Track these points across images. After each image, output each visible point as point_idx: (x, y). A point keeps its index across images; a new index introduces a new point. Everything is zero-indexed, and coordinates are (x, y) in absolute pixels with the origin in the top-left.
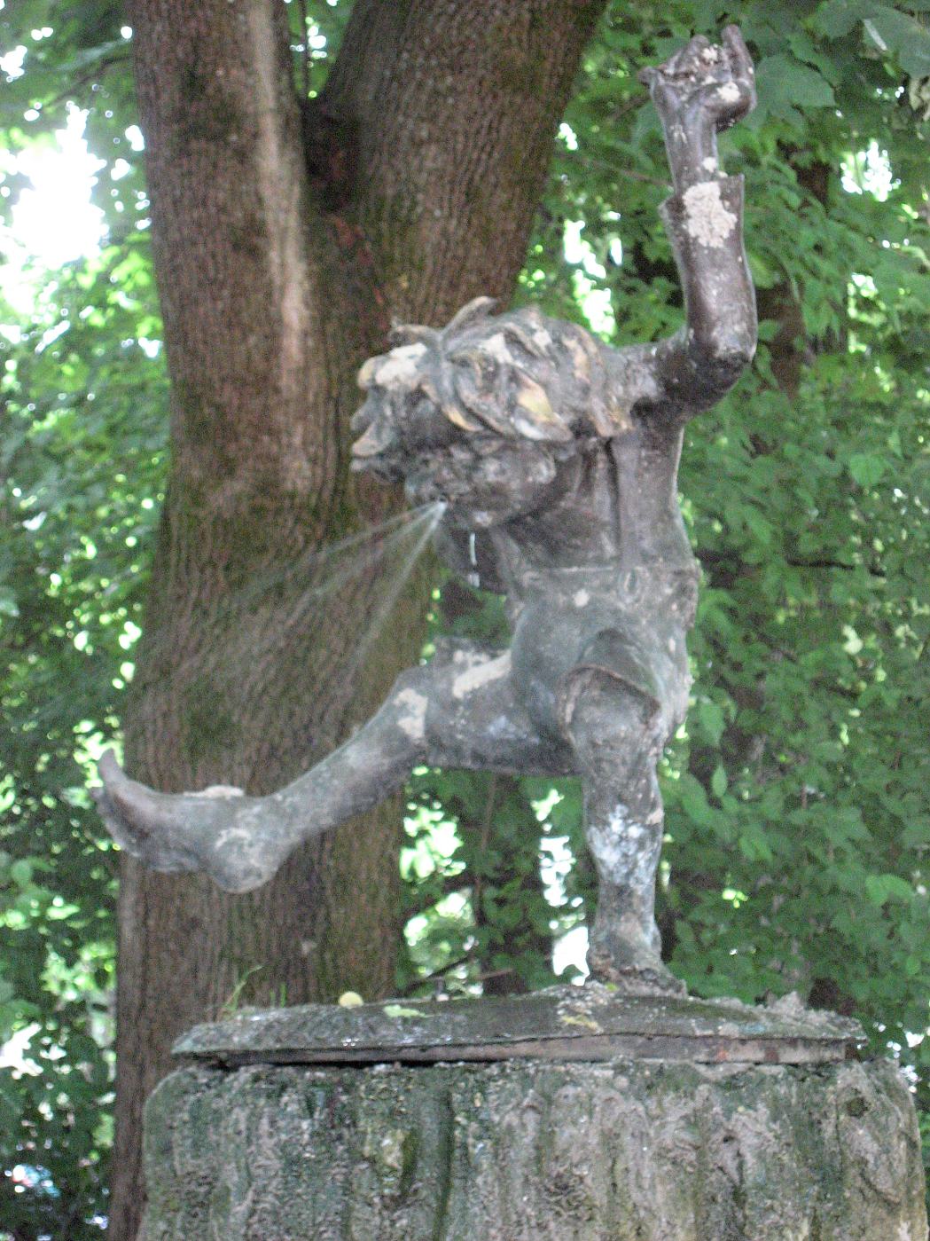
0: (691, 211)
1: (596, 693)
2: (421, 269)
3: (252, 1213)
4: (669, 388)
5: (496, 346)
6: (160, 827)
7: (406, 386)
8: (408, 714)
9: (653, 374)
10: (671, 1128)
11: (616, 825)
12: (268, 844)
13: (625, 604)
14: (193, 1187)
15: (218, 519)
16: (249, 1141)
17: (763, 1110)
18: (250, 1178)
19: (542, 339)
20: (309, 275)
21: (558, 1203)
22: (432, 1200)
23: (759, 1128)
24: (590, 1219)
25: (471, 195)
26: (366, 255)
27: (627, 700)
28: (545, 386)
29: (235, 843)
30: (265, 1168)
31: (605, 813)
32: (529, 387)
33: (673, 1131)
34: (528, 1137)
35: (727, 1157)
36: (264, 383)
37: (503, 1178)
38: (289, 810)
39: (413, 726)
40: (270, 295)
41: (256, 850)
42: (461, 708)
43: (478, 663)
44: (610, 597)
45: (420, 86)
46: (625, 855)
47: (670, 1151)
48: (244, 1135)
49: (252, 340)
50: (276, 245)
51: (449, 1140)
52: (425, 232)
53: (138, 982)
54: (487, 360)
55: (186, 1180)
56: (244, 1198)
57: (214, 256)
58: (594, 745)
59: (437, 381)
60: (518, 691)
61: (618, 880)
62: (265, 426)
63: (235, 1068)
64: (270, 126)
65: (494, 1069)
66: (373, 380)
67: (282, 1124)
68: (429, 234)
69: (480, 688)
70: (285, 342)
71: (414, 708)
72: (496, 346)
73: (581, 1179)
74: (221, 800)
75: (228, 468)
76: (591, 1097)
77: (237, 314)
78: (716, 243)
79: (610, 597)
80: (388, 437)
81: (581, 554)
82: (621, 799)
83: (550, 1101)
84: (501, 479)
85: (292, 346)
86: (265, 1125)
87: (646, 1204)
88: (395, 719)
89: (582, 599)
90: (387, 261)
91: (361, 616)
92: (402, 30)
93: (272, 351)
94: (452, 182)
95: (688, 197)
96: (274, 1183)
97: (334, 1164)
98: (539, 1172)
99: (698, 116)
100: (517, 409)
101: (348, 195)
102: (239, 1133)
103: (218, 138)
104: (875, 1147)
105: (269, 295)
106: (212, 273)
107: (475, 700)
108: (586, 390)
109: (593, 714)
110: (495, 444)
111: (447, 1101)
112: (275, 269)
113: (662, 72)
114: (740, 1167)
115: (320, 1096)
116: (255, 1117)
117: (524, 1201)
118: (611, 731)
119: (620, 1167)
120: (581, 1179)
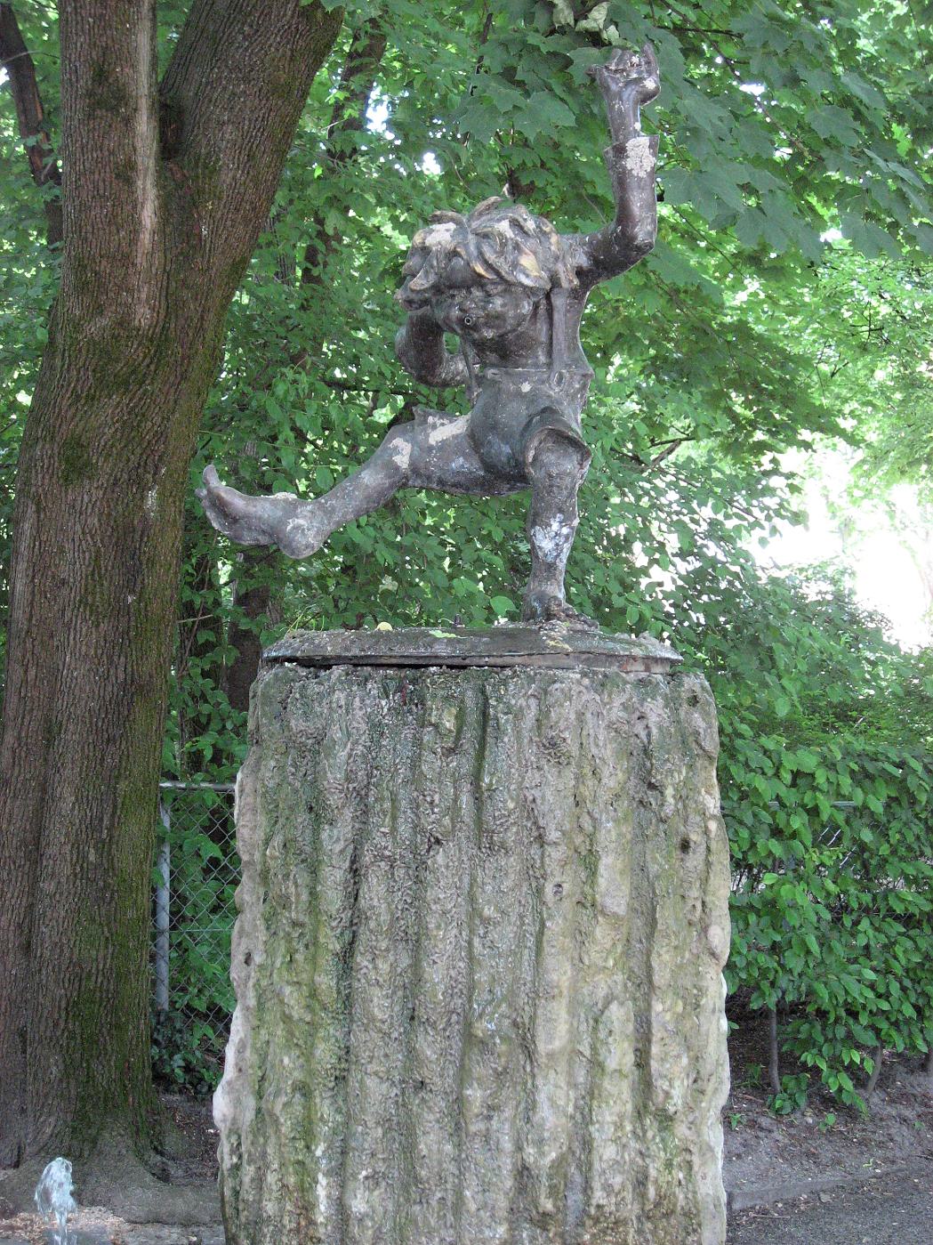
0: (630, 153)
2: (220, 199)
3: (350, 756)
4: (596, 262)
5: (504, 227)
6: (247, 516)
8: (398, 453)
9: (586, 253)
10: (615, 710)
11: (555, 526)
12: (319, 529)
13: (555, 391)
15: (92, 342)
16: (348, 713)
17: (660, 701)
18: (349, 735)
19: (530, 225)
20: (158, 197)
22: (471, 751)
23: (660, 712)
25: (250, 157)
26: (189, 188)
27: (571, 450)
28: (535, 253)
29: (296, 528)
30: (358, 729)
33: (616, 713)
34: (532, 714)
35: (639, 728)
36: (126, 260)
37: (519, 737)
39: (402, 461)
40: (136, 206)
41: (312, 533)
43: (443, 424)
44: (545, 388)
45: (225, 89)
46: (557, 545)
49: (122, 233)
50: (141, 177)
51: (484, 714)
52: (224, 177)
53: (27, 616)
54: (501, 234)
56: (345, 747)
57: (104, 181)
58: (550, 476)
59: (466, 246)
60: (475, 439)
61: (550, 559)
62: (124, 287)
63: (329, 667)
64: (144, 104)
65: (508, 672)
67: (368, 702)
68: (226, 178)
70: (142, 236)
72: (504, 227)
74: (286, 501)
75: (99, 310)
76: (570, 690)
77: (115, 217)
78: (643, 174)
79: (545, 388)
80: (432, 279)
82: (561, 511)
83: (546, 692)
84: (504, 310)
85: (146, 238)
86: (357, 702)
89: (526, 388)
90: (200, 192)
91: (171, 403)
92: (214, 56)
93: (134, 241)
94: (241, 148)
95: (629, 145)
98: (539, 736)
99: (631, 93)
101: (176, 151)
103: (114, 109)
104: (703, 725)
105: (135, 207)
106: (101, 192)
107: (443, 445)
108: (557, 259)
109: (550, 458)
110: (500, 288)
111: (483, 692)
112: (139, 192)
113: (607, 68)
114: (649, 735)
115: (392, 685)
116: (351, 696)
117: (531, 753)
118: (562, 468)
119: (584, 733)
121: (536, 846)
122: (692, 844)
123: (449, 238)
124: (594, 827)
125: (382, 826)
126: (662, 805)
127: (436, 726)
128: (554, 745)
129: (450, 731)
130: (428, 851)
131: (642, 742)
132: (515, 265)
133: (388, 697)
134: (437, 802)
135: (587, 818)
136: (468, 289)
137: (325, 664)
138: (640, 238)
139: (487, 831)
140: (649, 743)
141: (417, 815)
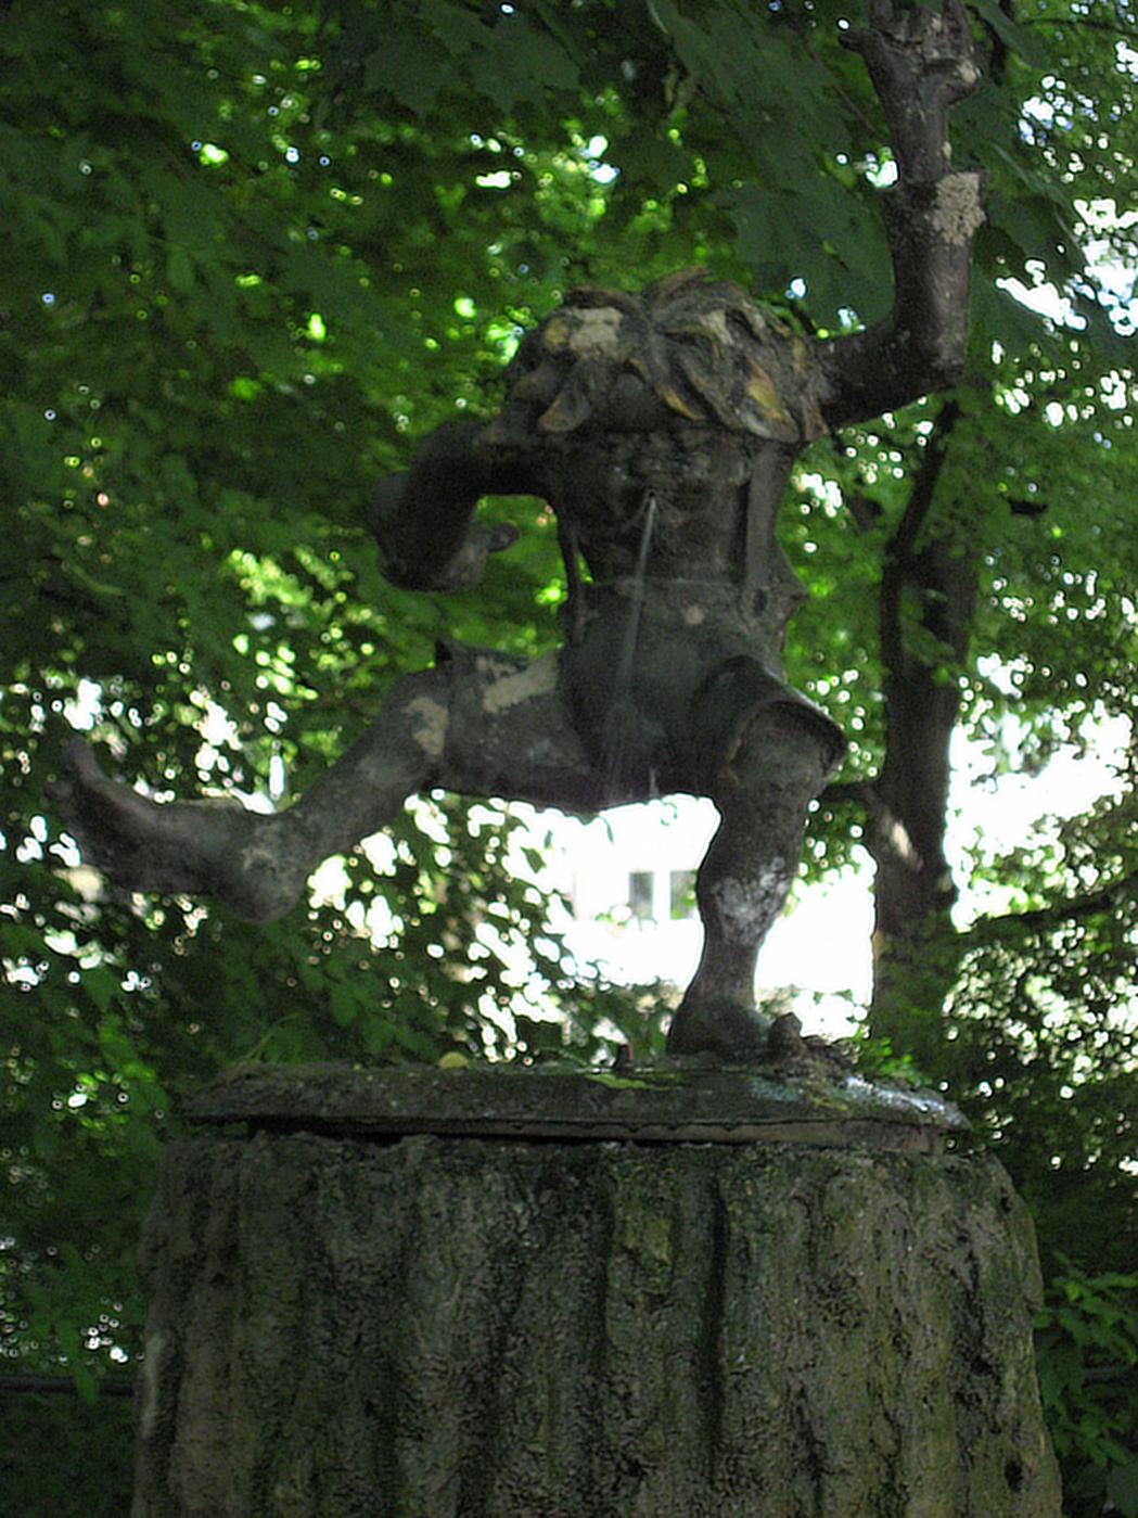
1: (770, 728)
5: (716, 322)
7: (609, 358)
14: (355, 1276)
21: (828, 1307)
24: (857, 1325)
27: (809, 739)
29: (260, 866)
31: (757, 865)
32: (758, 377)
38: (313, 830)
42: (495, 725)
43: (505, 674)
44: (730, 619)
47: (931, 1252)
48: (445, 1216)
51: (719, 1231)
55: (345, 1269)
59: (646, 354)
63: (395, 1138)
66: (567, 344)
69: (521, 703)
71: (431, 719)
72: (716, 322)
73: (854, 1280)
78: (959, 241)
80: (582, 412)
81: (685, 564)
86: (468, 1208)
87: (911, 1310)
88: (409, 731)
89: (695, 616)
96: (479, 1275)
97: (568, 1256)
98: (812, 1273)
100: (745, 400)
102: (438, 1215)
107: (512, 715)
114: (975, 1271)
120: (854, 1280)
121: (803, 1478)
122: (1025, 1474)
123: (613, 338)
124: (898, 1442)
125: (532, 1441)
126: (998, 1401)
127: (633, 1255)
128: (836, 1290)
129: (662, 1263)
130: (615, 1488)
131: (962, 1284)
132: (738, 396)
133: (525, 1198)
134: (637, 1395)
135: (884, 1424)
136: (645, 432)
137: (387, 1134)
138: (946, 355)
139: (729, 1449)
140: (975, 1285)
141: (591, 1421)
